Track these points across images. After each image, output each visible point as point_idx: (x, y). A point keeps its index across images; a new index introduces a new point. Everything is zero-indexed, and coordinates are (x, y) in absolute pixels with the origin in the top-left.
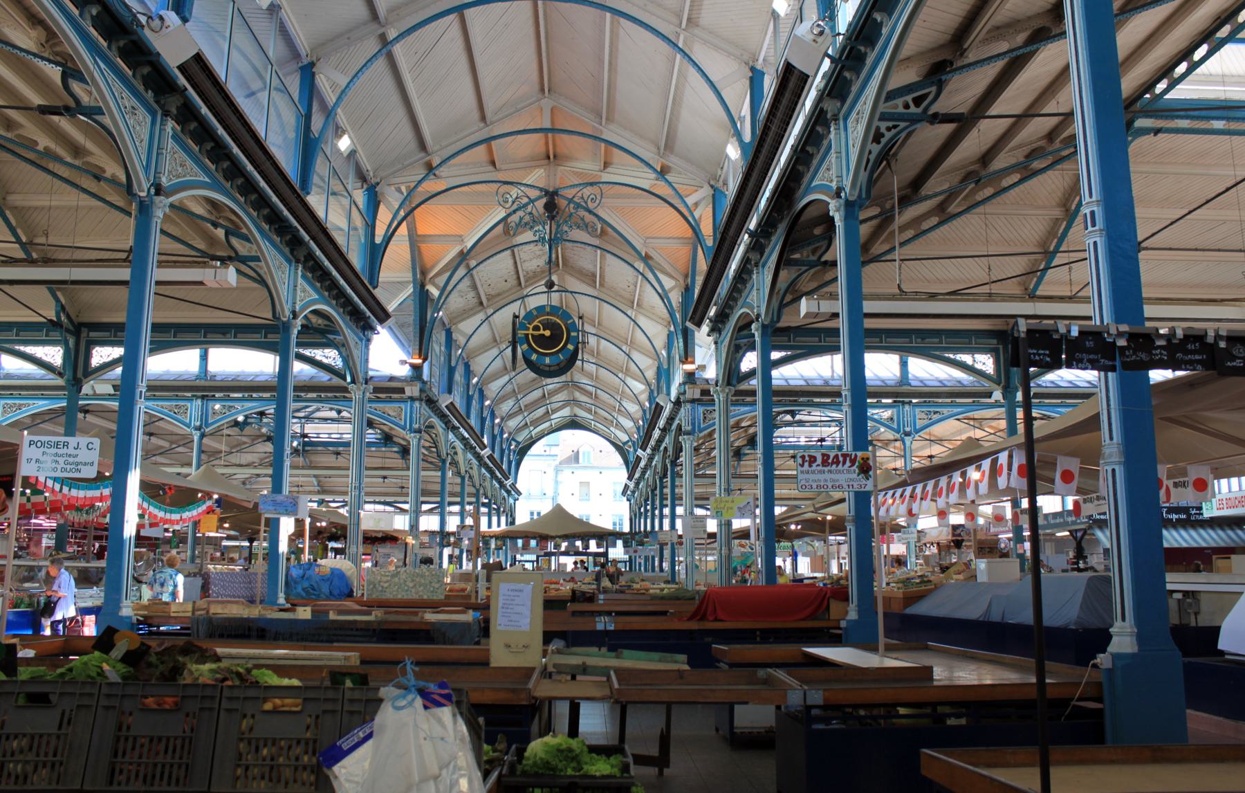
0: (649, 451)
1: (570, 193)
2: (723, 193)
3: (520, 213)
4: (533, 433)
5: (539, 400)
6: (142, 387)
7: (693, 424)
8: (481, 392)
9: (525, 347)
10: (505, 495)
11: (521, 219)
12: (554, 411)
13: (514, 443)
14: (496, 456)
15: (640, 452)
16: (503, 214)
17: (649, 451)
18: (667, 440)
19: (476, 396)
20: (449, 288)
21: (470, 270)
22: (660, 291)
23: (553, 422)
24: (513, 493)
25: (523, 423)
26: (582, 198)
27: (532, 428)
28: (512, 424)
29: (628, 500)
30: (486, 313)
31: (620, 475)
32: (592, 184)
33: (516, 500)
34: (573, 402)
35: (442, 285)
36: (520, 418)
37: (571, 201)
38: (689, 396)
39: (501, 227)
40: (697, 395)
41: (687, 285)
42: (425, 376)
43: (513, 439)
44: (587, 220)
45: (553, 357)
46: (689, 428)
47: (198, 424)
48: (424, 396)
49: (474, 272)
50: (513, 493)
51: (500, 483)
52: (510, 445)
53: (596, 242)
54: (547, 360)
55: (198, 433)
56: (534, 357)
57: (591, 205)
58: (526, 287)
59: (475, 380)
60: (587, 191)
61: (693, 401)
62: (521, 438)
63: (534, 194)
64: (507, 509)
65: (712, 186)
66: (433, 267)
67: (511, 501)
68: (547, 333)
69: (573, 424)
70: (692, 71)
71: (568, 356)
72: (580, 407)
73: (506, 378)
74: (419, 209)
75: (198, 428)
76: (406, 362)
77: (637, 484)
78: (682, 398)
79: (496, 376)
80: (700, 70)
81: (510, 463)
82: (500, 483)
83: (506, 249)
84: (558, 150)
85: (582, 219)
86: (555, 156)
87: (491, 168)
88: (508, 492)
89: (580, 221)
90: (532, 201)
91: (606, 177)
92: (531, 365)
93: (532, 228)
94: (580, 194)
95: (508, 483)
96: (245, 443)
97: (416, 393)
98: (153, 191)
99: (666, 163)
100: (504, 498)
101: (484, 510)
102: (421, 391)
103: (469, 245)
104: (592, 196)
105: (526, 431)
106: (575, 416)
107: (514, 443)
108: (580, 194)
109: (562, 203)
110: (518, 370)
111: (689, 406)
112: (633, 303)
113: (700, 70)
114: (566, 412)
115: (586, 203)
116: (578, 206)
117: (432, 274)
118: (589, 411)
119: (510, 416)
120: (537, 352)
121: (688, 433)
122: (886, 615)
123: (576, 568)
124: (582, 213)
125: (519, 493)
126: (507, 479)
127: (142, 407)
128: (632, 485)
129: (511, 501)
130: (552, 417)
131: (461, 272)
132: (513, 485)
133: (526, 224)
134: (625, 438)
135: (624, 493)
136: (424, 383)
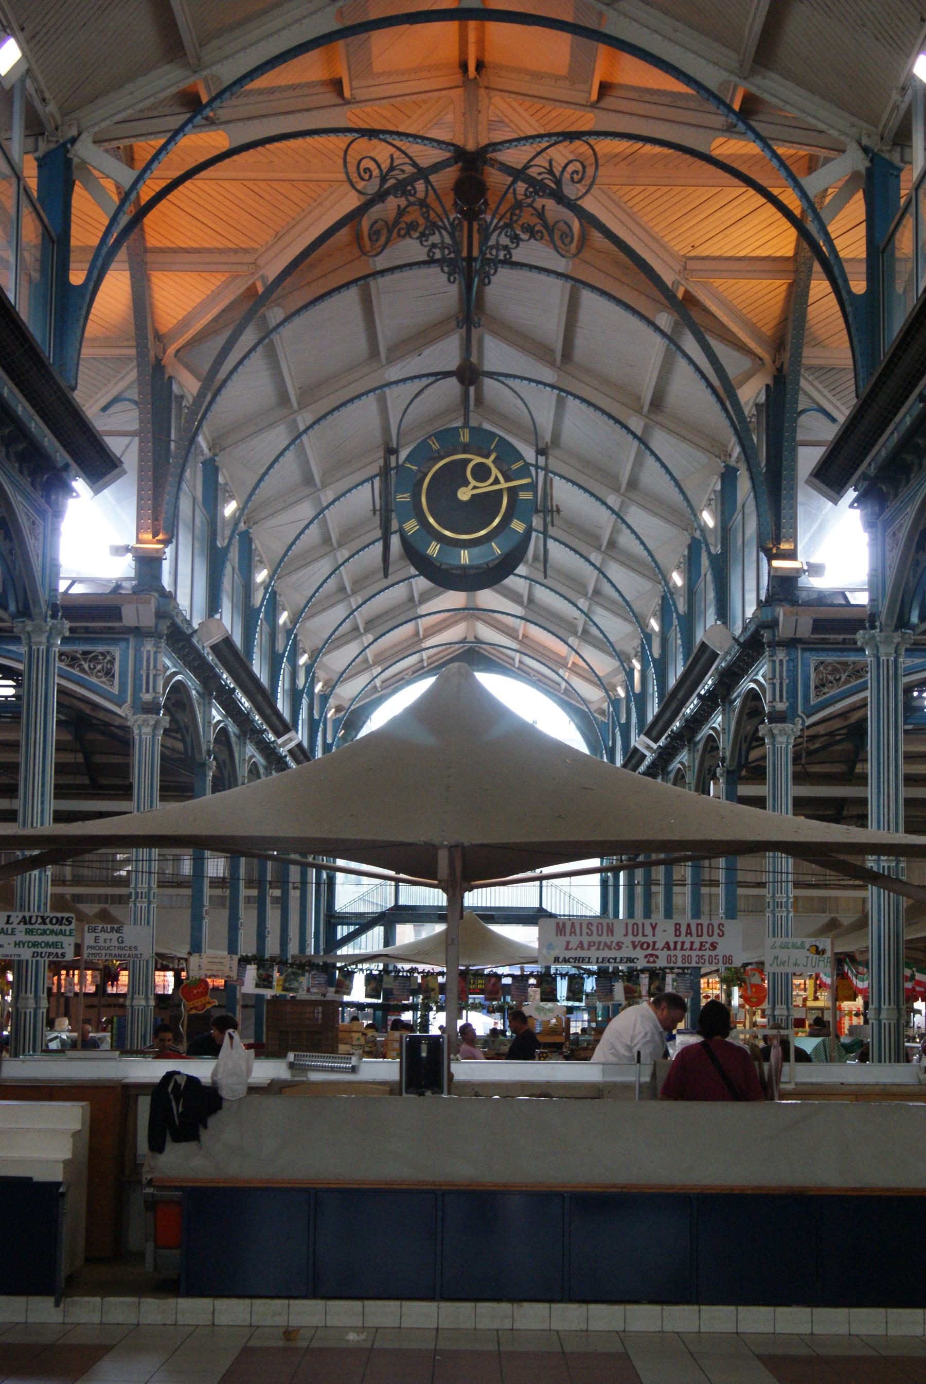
1: (515, 157)
3: (393, 203)
7: (793, 695)
8: (246, 540)
9: (411, 526)
11: (401, 212)
12: (431, 631)
16: (352, 201)
18: (717, 720)
19: (234, 555)
20: (222, 375)
22: (716, 382)
23: (425, 655)
25: (346, 626)
26: (551, 172)
30: (350, 605)
35: (206, 367)
36: (324, 567)
37: (518, 174)
38: (784, 631)
39: (344, 234)
40: (805, 630)
41: (780, 370)
44: (551, 217)
45: (476, 550)
46: (781, 706)
48: (164, 627)
49: (275, 337)
54: (465, 557)
56: (434, 549)
57: (570, 191)
58: (390, 361)
59: (230, 509)
60: (561, 154)
61: (791, 644)
63: (428, 156)
65: (866, 150)
68: (464, 494)
70: (650, 460)
71: (511, 544)
74: (389, 278)
78: (766, 636)
80: (658, 459)
83: (347, 285)
84: (488, 58)
85: (541, 215)
86: (480, 66)
87: (331, 98)
89: (534, 220)
90: (422, 173)
92: (426, 567)
93: (423, 237)
94: (541, 161)
97: (148, 620)
98: (50, 613)
99: (753, 90)
102: (161, 615)
106: (478, 641)
108: (541, 161)
109: (495, 179)
110: (392, 579)
111: (781, 655)
113: (658, 459)
115: (558, 182)
116: (537, 187)
118: (511, 633)
119: (333, 642)
120: (441, 539)
121: (778, 717)
123: (500, 1009)
124: (550, 204)
126: (283, 727)
131: (248, 338)
133: (412, 226)
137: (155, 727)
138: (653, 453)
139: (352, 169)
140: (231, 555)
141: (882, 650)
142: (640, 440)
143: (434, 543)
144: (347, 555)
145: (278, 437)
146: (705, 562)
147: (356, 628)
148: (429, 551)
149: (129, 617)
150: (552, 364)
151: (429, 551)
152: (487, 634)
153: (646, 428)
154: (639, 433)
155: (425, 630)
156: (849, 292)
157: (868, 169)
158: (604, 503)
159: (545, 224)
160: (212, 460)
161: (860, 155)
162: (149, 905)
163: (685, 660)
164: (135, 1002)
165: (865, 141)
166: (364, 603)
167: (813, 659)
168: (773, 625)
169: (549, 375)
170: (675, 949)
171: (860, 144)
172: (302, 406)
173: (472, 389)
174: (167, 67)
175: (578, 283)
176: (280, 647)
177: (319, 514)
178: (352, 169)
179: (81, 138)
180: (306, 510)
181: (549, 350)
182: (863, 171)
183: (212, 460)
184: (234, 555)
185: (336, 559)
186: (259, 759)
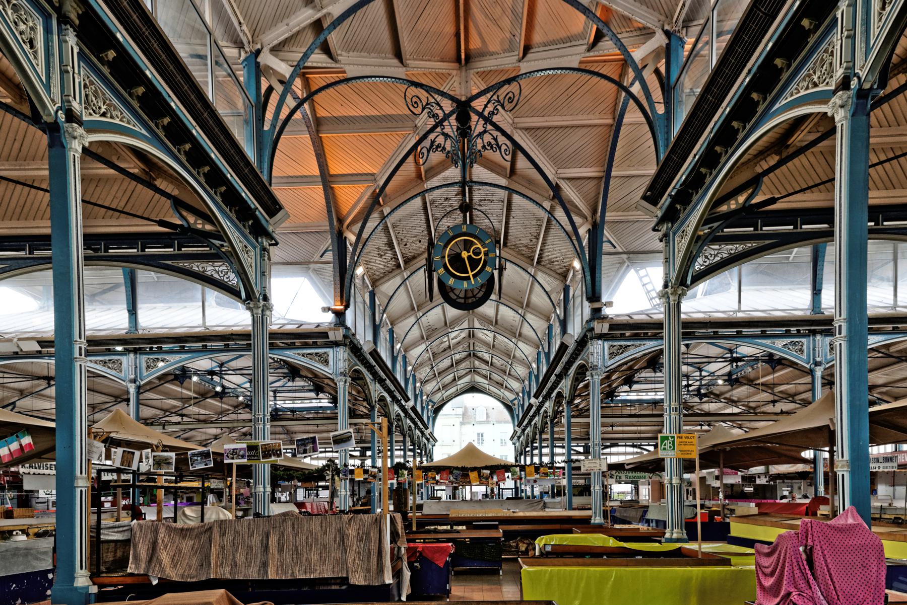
0: (541, 399)
2: (681, 39)
4: (444, 396)
5: (448, 368)
6: (80, 344)
9: (441, 271)
10: (426, 442)
13: (431, 404)
14: (419, 409)
15: (533, 400)
17: (541, 399)
19: (411, 380)
21: (383, 218)
24: (431, 440)
26: (498, 101)
27: (444, 392)
28: (429, 388)
29: (514, 444)
31: (509, 428)
32: (509, 81)
33: (433, 446)
34: (473, 371)
35: (357, 232)
36: (434, 383)
40: (606, 330)
42: (349, 322)
43: (430, 400)
47: (133, 377)
48: (348, 341)
50: (431, 440)
51: (422, 433)
52: (428, 405)
53: (503, 182)
55: (133, 385)
62: (437, 398)
64: (428, 451)
66: (349, 213)
67: (430, 446)
69: (473, 389)
70: (537, 284)
72: (479, 374)
73: (423, 347)
75: (134, 381)
76: (329, 309)
77: (523, 431)
78: (589, 335)
79: (415, 344)
81: (428, 418)
82: (422, 433)
83: (415, 196)
87: (395, 62)
88: (428, 440)
91: (525, 67)
92: (447, 294)
95: (427, 432)
96: (229, 410)
100: (425, 444)
101: (411, 453)
102: (345, 336)
103: (381, 183)
104: (511, 95)
105: (440, 394)
107: (431, 404)
112: (533, 260)
114: (467, 379)
117: (348, 221)
122: (702, 523)
125: (435, 440)
127: (84, 364)
128: (519, 431)
129: (430, 446)
130: (459, 383)
132: (431, 434)
134: (511, 396)
135: (512, 438)
136: (348, 329)
137: (345, 382)
138: (538, 281)
139: (409, 100)
140: (399, 358)
141: (672, 298)
142: (533, 277)
143: (452, 279)
144: (421, 315)
145: (412, 320)
146: (533, 377)
147: (440, 389)
148: (450, 283)
149: (332, 337)
150: (505, 176)
151: (450, 283)
152: (478, 379)
153: (524, 313)
154: (548, 209)
155: (426, 172)
156: (656, 112)
157: (667, 45)
158: (527, 271)
159: (497, 145)
160: (373, 291)
161: (663, 37)
162: (264, 427)
163: (547, 366)
164: (257, 490)
165: (667, 27)
166: (411, 274)
167: (607, 345)
168: (593, 329)
169: (503, 182)
170: (409, 541)
171: (663, 30)
172: (418, 310)
173: (468, 214)
174: (305, 9)
175: (511, 191)
176: (417, 392)
177: (382, 220)
178: (409, 100)
179: (263, 50)
180: (412, 320)
181: (488, 363)
182: (665, 46)
183: (373, 291)
184: (411, 380)
185: (417, 316)
186: (420, 435)
